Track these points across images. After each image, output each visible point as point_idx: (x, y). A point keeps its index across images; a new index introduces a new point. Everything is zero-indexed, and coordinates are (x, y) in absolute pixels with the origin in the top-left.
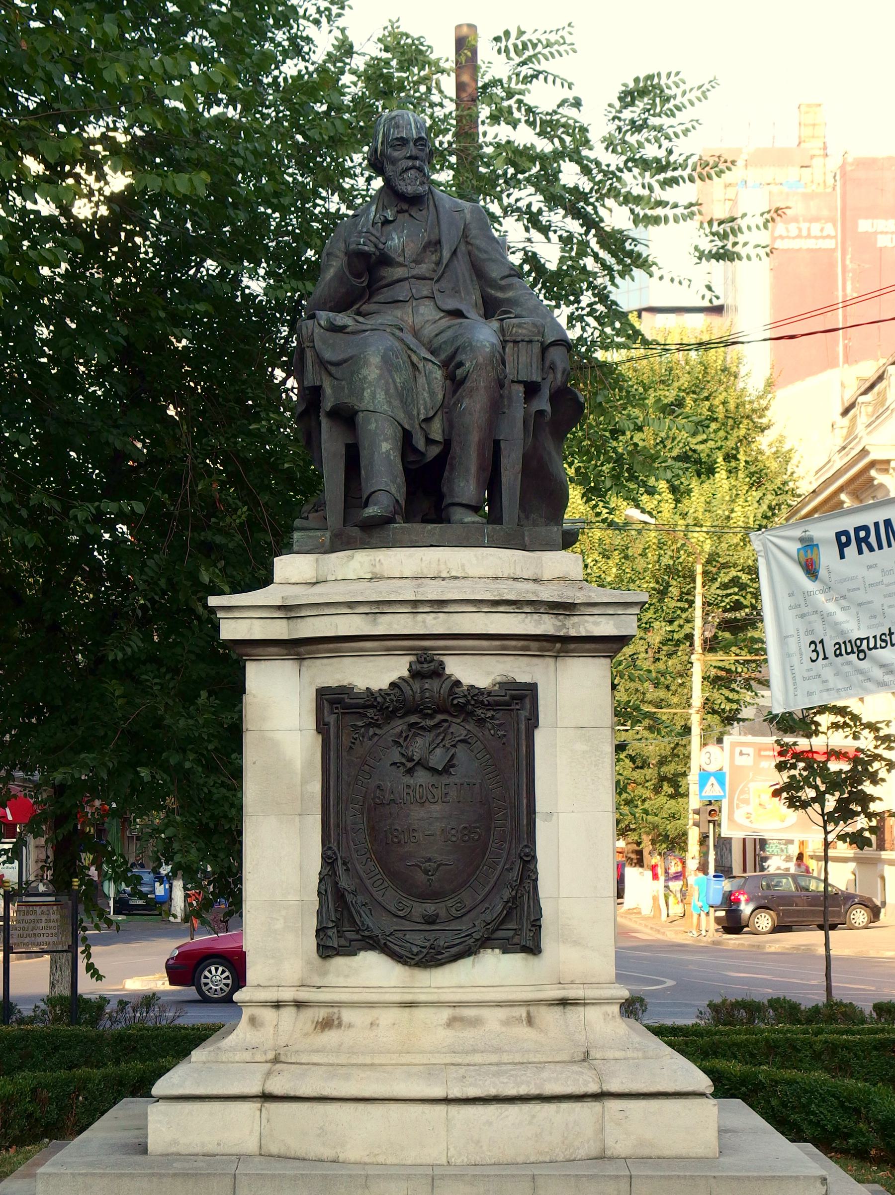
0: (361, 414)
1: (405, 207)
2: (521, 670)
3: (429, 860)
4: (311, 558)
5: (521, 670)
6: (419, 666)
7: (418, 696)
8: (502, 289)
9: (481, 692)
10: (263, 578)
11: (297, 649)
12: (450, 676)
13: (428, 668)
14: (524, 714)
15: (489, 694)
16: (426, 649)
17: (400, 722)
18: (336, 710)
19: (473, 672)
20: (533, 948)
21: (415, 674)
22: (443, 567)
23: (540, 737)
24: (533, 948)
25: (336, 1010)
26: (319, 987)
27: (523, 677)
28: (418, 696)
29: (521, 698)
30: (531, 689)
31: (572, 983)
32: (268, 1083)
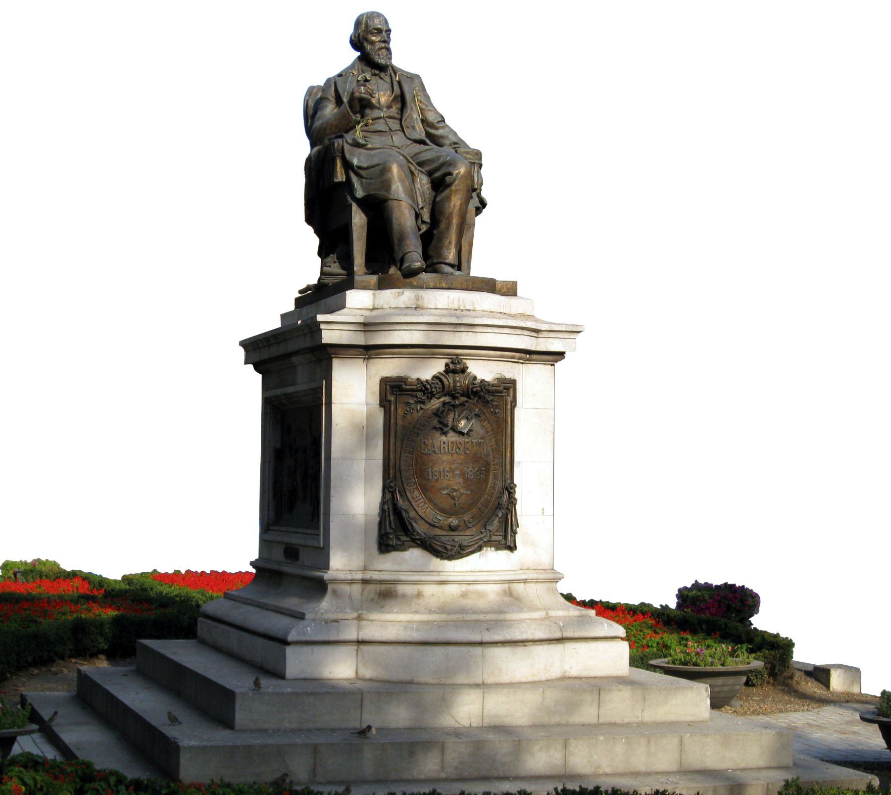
0: (390, 202)
1: (377, 72)
2: (507, 370)
3: (456, 491)
4: (370, 293)
5: (507, 370)
6: (451, 366)
7: (452, 385)
8: (437, 129)
9: (489, 384)
10: (341, 306)
11: (369, 352)
12: (470, 373)
13: (456, 368)
14: (509, 399)
15: (493, 386)
16: (457, 355)
17: (438, 401)
18: (393, 391)
19: (483, 371)
20: (512, 548)
21: (448, 371)
22: (461, 303)
23: (517, 411)
24: (512, 548)
25: (392, 586)
26: (380, 571)
27: (508, 376)
28: (452, 385)
29: (507, 389)
30: (513, 382)
31: (528, 569)
32: (361, 633)
